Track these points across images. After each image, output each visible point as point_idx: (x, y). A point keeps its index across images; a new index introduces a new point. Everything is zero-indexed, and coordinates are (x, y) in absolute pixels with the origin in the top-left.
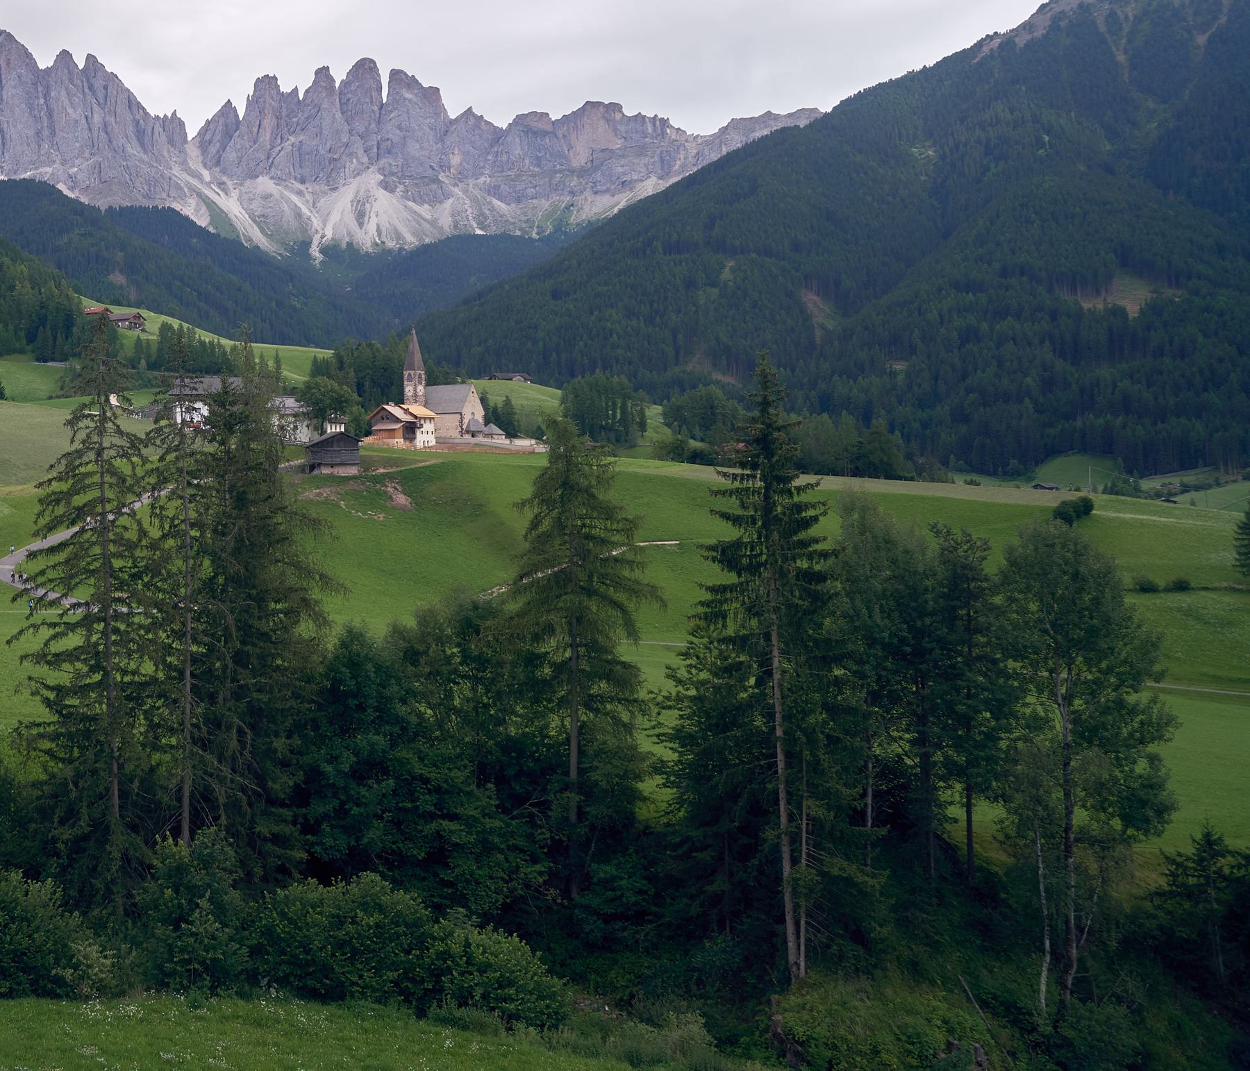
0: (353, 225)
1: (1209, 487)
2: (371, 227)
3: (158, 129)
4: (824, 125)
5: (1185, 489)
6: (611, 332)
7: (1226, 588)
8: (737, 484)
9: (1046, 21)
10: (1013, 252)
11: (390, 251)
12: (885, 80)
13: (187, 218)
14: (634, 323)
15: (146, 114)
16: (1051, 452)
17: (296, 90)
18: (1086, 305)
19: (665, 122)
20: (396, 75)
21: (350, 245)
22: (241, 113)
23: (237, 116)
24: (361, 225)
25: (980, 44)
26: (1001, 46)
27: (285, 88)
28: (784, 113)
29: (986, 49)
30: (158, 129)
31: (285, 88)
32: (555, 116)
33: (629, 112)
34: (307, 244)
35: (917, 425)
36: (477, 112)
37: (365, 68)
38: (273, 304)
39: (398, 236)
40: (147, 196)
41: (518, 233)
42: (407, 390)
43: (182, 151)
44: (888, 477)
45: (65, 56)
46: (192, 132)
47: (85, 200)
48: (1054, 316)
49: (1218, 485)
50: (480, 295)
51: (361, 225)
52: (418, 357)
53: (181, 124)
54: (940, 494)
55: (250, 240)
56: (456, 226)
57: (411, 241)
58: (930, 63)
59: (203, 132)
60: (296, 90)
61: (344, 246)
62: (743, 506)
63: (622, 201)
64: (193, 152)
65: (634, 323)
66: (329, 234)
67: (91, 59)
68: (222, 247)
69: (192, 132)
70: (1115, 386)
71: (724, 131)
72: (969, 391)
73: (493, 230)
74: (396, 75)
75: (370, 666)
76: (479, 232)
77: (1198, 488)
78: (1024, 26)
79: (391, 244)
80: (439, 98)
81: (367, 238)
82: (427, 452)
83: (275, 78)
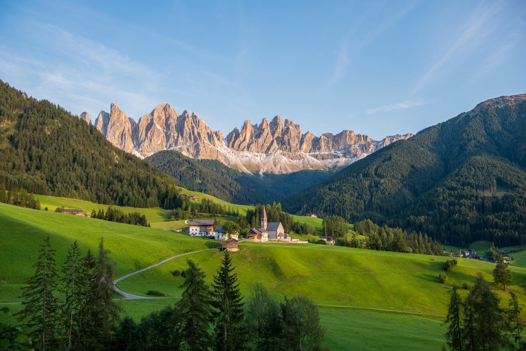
0: (273, 166)
1: (517, 251)
2: (278, 166)
5: (511, 252)
6: (346, 201)
7: (152, 236)
10: (466, 178)
11: (284, 174)
14: (353, 198)
17: (256, 125)
24: (275, 166)
25: (459, 116)
26: (465, 117)
29: (461, 117)
38: (247, 190)
39: (286, 170)
50: (308, 189)
51: (275, 166)
56: (304, 167)
57: (290, 171)
60: (256, 125)
65: (353, 198)
67: (59, 106)
70: (493, 220)
72: (451, 221)
73: (315, 169)
75: (451, 338)
76: (311, 169)
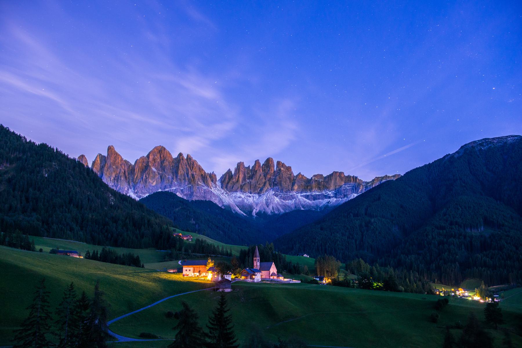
0: (265, 207)
3: (208, 177)
4: (401, 179)
8: (213, 326)
12: (409, 170)
13: (215, 204)
15: (205, 173)
17: (249, 166)
19: (356, 178)
20: (278, 163)
21: (264, 212)
22: (233, 173)
23: (232, 173)
24: (268, 206)
25: (444, 157)
27: (246, 165)
28: (391, 175)
30: (208, 177)
31: (246, 165)
32: (324, 176)
33: (346, 175)
34: (251, 212)
36: (302, 174)
37: (269, 161)
38: (240, 230)
39: (279, 210)
42: (255, 264)
43: (215, 183)
44: (391, 291)
45: (180, 154)
46: (218, 178)
47: (185, 198)
48: (465, 237)
51: (268, 206)
52: (258, 254)
53: (215, 175)
55: (234, 210)
59: (222, 178)
60: (249, 166)
62: (210, 332)
63: (345, 200)
64: (218, 183)
68: (226, 212)
69: (218, 178)
70: (482, 259)
71: (373, 180)
73: (307, 209)
74: (278, 163)
78: (457, 152)
79: (276, 212)
80: (291, 170)
82: (258, 283)
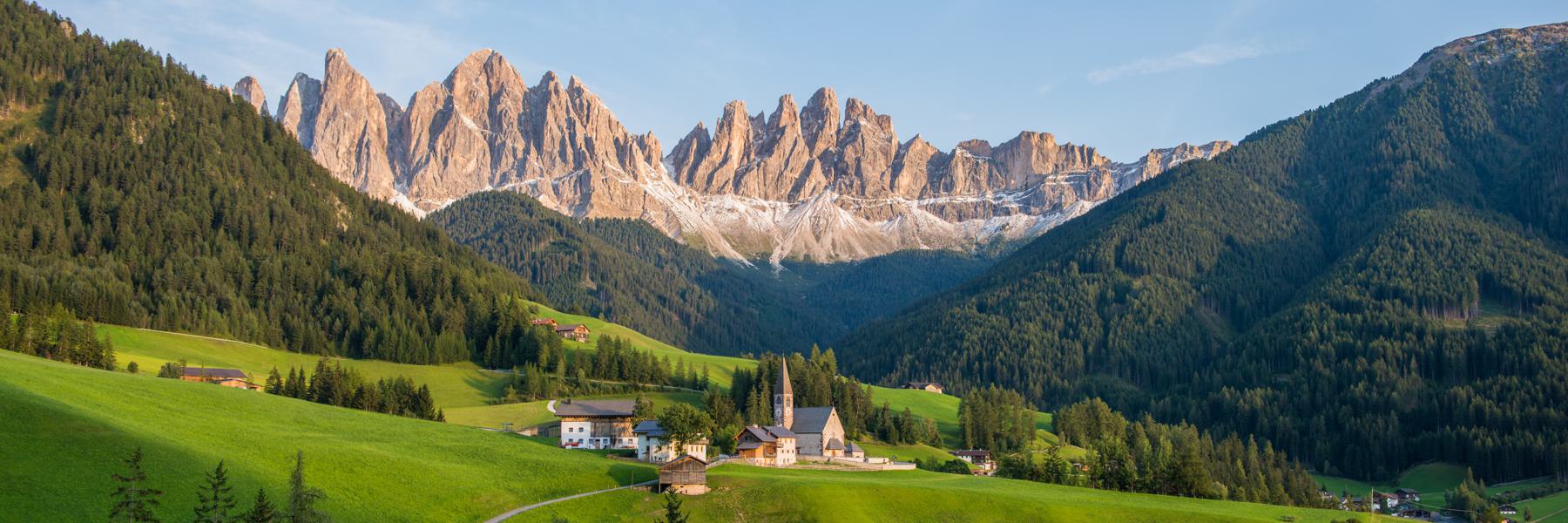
0: (811, 239)
1: (1542, 495)
2: (827, 240)
5: (1524, 497)
6: (1029, 343)
9: (1426, 69)
11: (843, 264)
14: (1049, 335)
16: (1414, 458)
17: (762, 115)
18: (1448, 326)
21: (807, 256)
24: (818, 238)
25: (1368, 88)
26: (1386, 90)
29: (1374, 92)
32: (994, 144)
35: (1296, 433)
39: (851, 249)
40: (624, 209)
41: (959, 249)
49: (1552, 492)
51: (818, 238)
54: (1235, 515)
56: (903, 242)
57: (863, 254)
58: (1326, 104)
60: (762, 115)
61: (801, 258)
65: (1049, 335)
66: (789, 246)
72: (1343, 402)
77: (1534, 496)
81: (821, 255)
83: (888, 119)
